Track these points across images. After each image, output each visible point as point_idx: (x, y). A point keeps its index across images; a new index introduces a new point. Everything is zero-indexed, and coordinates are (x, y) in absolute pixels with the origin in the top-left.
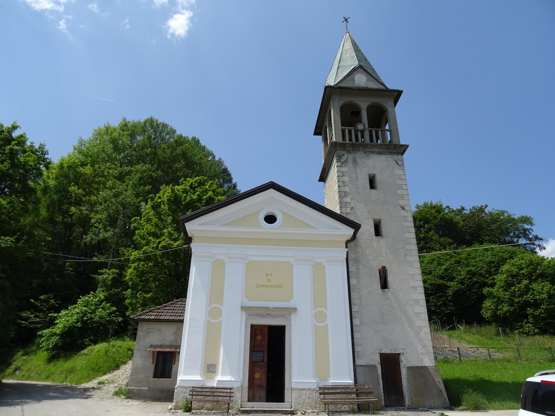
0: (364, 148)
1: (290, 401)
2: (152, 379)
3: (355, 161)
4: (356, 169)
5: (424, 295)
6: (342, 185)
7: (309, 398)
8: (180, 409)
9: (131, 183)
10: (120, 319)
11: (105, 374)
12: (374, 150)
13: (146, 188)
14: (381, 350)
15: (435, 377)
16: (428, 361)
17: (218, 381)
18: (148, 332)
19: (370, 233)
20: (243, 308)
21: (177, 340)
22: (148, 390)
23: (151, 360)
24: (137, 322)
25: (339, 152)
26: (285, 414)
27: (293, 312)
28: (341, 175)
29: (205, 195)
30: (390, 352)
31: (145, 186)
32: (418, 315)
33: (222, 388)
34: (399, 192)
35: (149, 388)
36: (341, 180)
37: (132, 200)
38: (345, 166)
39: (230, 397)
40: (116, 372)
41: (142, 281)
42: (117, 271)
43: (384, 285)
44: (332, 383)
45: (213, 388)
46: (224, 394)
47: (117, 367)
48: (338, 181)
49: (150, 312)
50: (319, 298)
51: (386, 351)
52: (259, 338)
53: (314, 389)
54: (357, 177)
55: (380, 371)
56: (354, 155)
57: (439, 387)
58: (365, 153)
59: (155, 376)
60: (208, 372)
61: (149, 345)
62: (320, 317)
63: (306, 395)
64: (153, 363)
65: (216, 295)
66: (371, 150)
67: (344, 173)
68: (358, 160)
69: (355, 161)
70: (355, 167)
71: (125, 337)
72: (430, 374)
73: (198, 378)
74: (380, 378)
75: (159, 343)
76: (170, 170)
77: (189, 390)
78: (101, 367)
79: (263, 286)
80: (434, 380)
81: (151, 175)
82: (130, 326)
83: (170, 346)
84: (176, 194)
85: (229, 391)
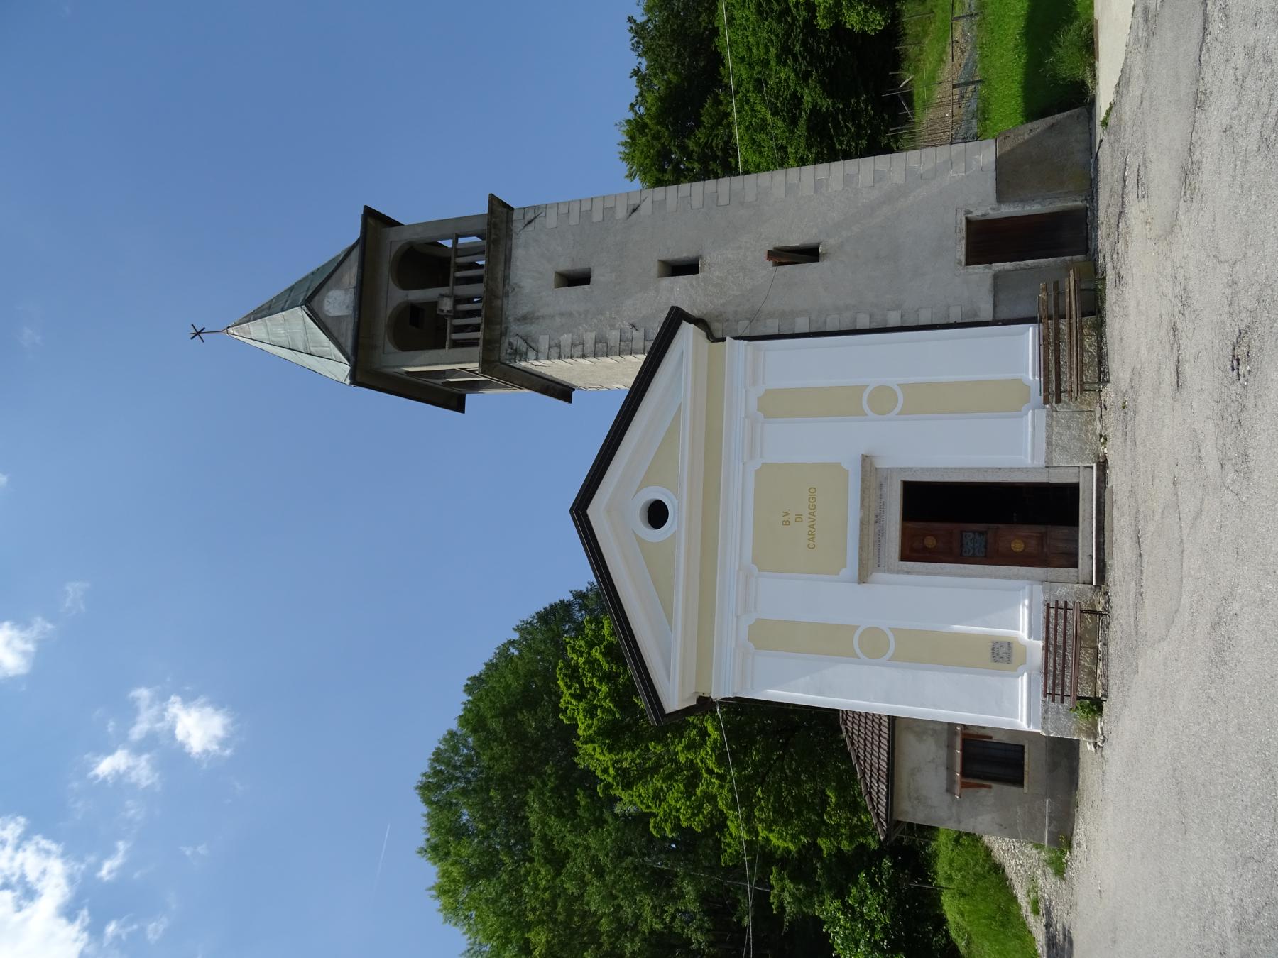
0: (497, 297)
1: (1076, 470)
2: (1026, 790)
3: (524, 319)
4: (543, 317)
7: (1069, 428)
10: (887, 863)
11: (1014, 899)
12: (500, 275)
13: (582, 803)
14: (959, 263)
15: (1021, 139)
16: (985, 155)
17: (1030, 636)
18: (917, 799)
20: (863, 578)
22: (1052, 797)
23: (983, 791)
24: (893, 823)
27: (871, 464)
30: (963, 242)
32: (878, 177)
33: (1047, 628)
34: (597, 217)
37: (610, 834)
38: (536, 341)
39: (1066, 608)
40: (1010, 872)
41: (799, 813)
42: (774, 869)
43: (810, 254)
44: (1034, 375)
45: (1046, 648)
46: (1061, 622)
47: (998, 869)
48: (571, 357)
49: (870, 793)
52: (930, 542)
54: (562, 315)
55: (1008, 265)
56: (511, 319)
58: (506, 295)
59: (1019, 782)
60: (1009, 660)
61: (948, 797)
62: (882, 400)
63: (1061, 435)
64: (990, 787)
65: (832, 642)
69: (524, 319)
70: (538, 318)
72: (1013, 150)
73: (1023, 682)
74: (1022, 263)
75: (943, 772)
76: (543, 744)
77: (1052, 705)
78: (999, 908)
79: (811, 534)
83: (951, 747)
85: (1052, 611)
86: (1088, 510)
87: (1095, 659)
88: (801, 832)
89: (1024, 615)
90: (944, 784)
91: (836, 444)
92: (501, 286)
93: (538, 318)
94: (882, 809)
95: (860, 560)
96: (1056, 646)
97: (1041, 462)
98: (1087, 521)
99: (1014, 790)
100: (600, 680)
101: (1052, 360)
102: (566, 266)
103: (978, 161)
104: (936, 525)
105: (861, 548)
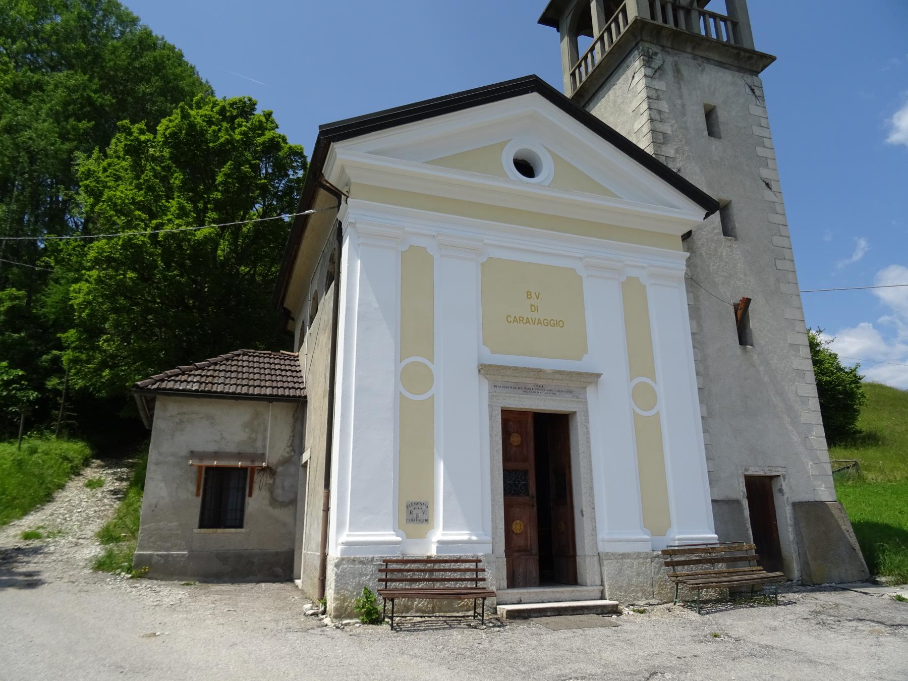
0: (694, 48)
1: (598, 582)
2: (197, 531)
3: (677, 71)
4: (680, 88)
5: (811, 361)
6: (658, 117)
7: (638, 575)
8: (350, 616)
9: (46, 107)
10: (33, 395)
11: (25, 512)
12: (711, 55)
13: (80, 125)
14: (746, 470)
15: (841, 523)
16: (825, 492)
17: (439, 542)
18: (181, 421)
19: (714, 228)
20: (485, 369)
21: (255, 441)
22: (190, 557)
23: (193, 488)
24: (151, 397)
25: (647, 45)
26: (603, 613)
27: (591, 383)
28: (655, 96)
29: (260, 135)
30: (762, 473)
31: (80, 121)
32: (804, 400)
33: (456, 561)
34: (760, 151)
35: (191, 551)
36: (655, 106)
37: (52, 144)
38: (660, 78)
39: (477, 580)
40: (49, 508)
41: (115, 310)
42: (22, 293)
43: (744, 336)
44: (679, 540)
45: (429, 560)
46: (457, 575)
47: (48, 498)
48: (650, 108)
49: (183, 374)
50: (640, 359)
51: (756, 471)
52: (516, 439)
53: (647, 553)
54: (683, 106)
55: (747, 513)
56: (676, 58)
57: (849, 542)
58: (695, 57)
59: (201, 526)
60: (409, 521)
61: (184, 452)
62: (644, 396)
63: (631, 567)
64: (198, 495)
65: (414, 335)
66: (706, 54)
67: (660, 93)
68: (684, 70)
69: (677, 71)
70: (679, 83)
71: (47, 433)
72: (832, 515)
73: (390, 536)
74: (749, 525)
75: (212, 448)
76: (130, 99)
77: (370, 568)
78: (14, 498)
79: (521, 320)
80: (841, 528)
81: (89, 97)
82: (58, 409)
83: (239, 456)
84: (192, 126)
85: (472, 566)
86: (563, 597)
87: (422, 612)
88: (93, 310)
89: (462, 535)
90: (200, 447)
91: (603, 347)
92: (702, 54)
93: (679, 83)
94: (170, 385)
95: (505, 368)
96: (432, 571)
97: (603, 548)
98: (566, 596)
99: (196, 520)
100: (244, 134)
101: (694, 557)
102: (722, 115)
103: (820, 486)
104: (532, 444)
105: (516, 369)
